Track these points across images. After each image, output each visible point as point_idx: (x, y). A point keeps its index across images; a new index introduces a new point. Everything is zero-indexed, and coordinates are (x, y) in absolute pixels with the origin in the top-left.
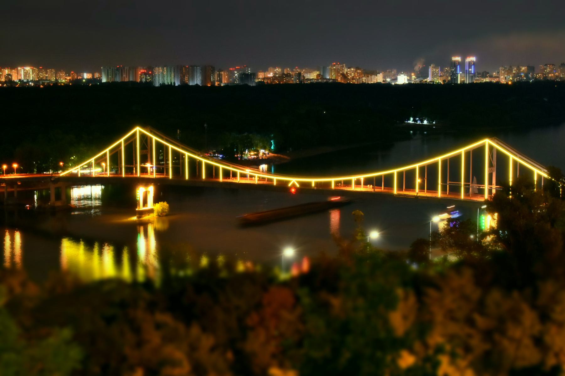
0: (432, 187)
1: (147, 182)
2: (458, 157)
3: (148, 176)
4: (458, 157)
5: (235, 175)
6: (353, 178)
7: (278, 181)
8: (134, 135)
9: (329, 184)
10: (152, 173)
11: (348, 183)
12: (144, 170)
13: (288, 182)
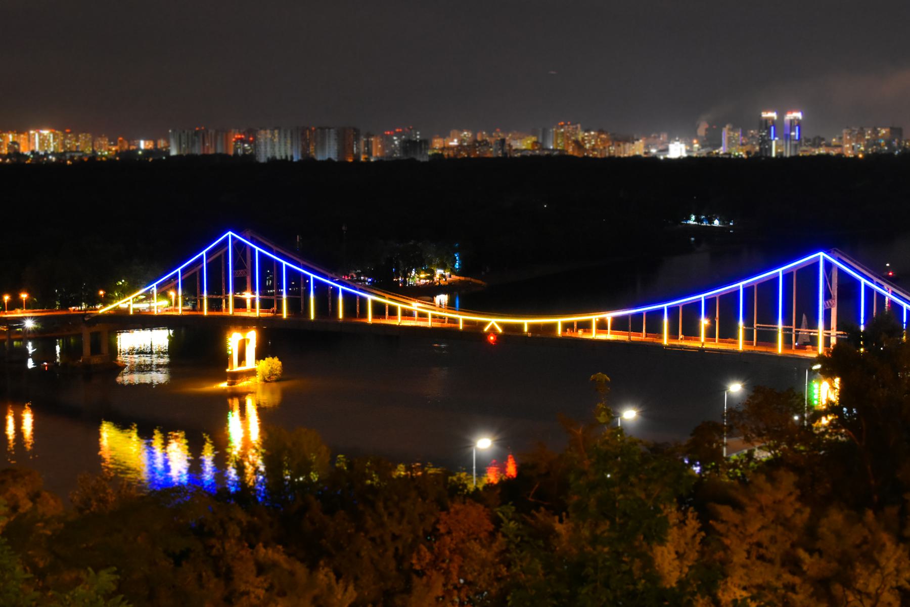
0: (728, 333)
1: (244, 323)
2: (775, 279)
3: (248, 313)
4: (775, 279)
5: (393, 312)
6: (594, 318)
7: (533, 328)
8: (227, 238)
9: (553, 327)
10: (253, 306)
11: (586, 326)
12: (240, 304)
13: (553, 327)
